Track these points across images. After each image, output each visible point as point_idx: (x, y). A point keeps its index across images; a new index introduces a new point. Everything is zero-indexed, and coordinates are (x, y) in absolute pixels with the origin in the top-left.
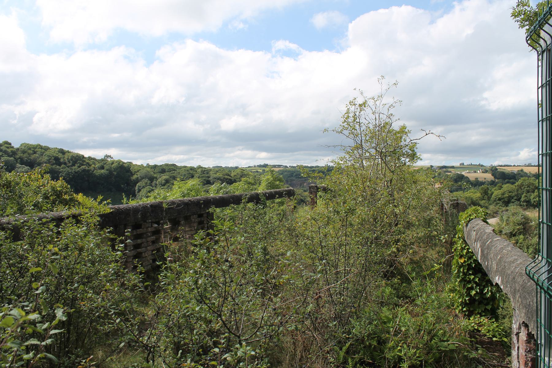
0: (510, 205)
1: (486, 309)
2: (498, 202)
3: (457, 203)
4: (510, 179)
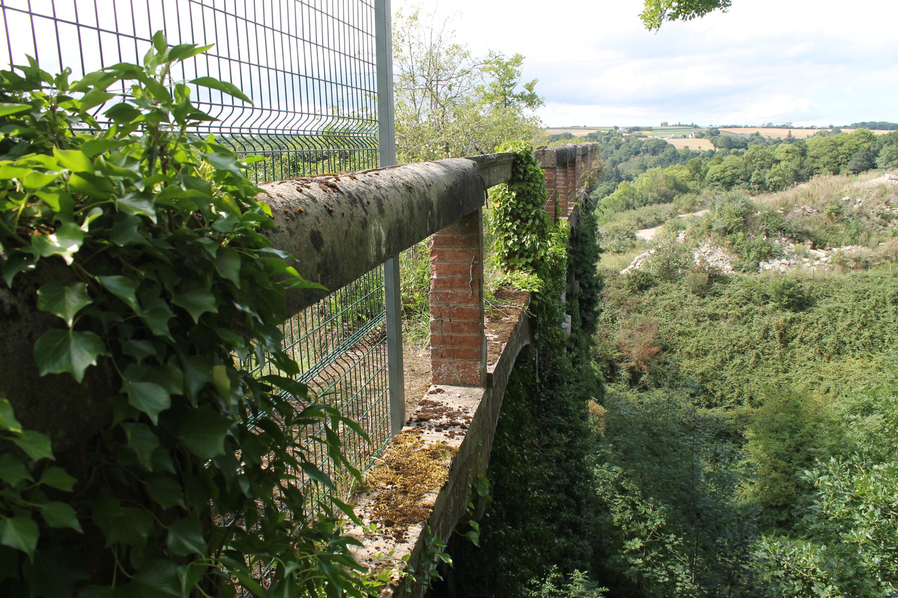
0: (733, 188)
1: (527, 263)
2: (717, 183)
3: (544, 151)
4: (739, 148)
